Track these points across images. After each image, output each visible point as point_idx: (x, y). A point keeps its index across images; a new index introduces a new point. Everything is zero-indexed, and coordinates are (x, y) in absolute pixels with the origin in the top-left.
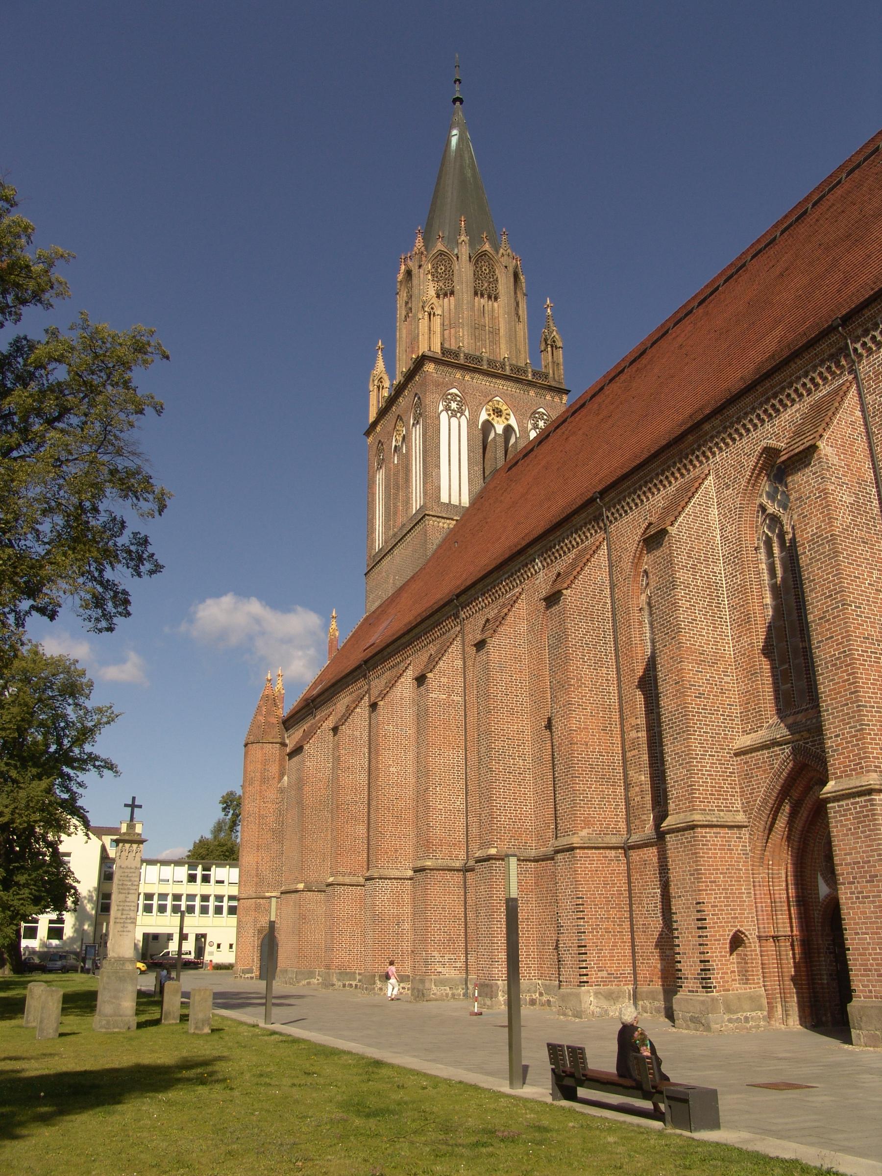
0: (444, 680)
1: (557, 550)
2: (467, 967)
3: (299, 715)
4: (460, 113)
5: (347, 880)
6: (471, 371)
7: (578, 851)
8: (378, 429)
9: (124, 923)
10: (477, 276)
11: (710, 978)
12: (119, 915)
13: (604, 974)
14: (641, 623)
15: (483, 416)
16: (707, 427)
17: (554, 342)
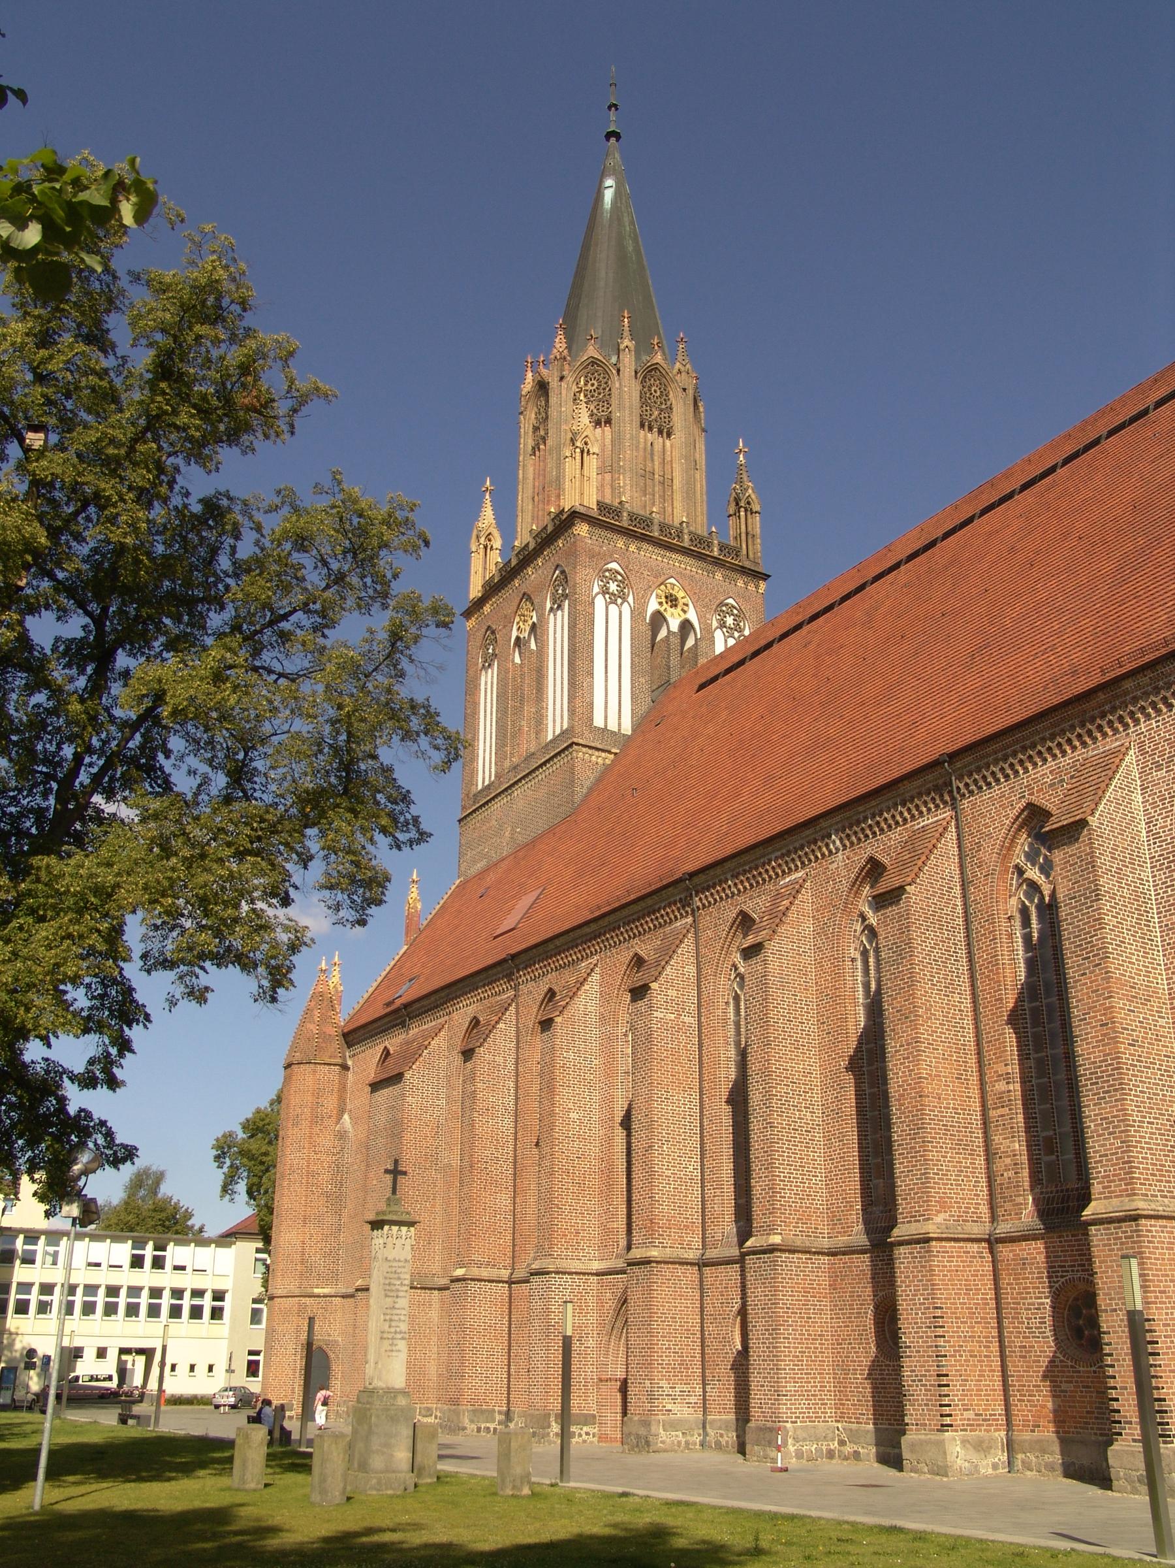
0: (672, 993)
1: (870, 826)
2: (704, 1404)
3: (375, 1025)
4: (617, 155)
5: (485, 1273)
6: (636, 538)
7: (934, 1243)
8: (487, 609)
9: (393, 1338)
10: (644, 400)
11: (1168, 1424)
12: (386, 1328)
13: (970, 1414)
14: (1010, 936)
15: (653, 606)
16: (1128, 685)
17: (749, 503)
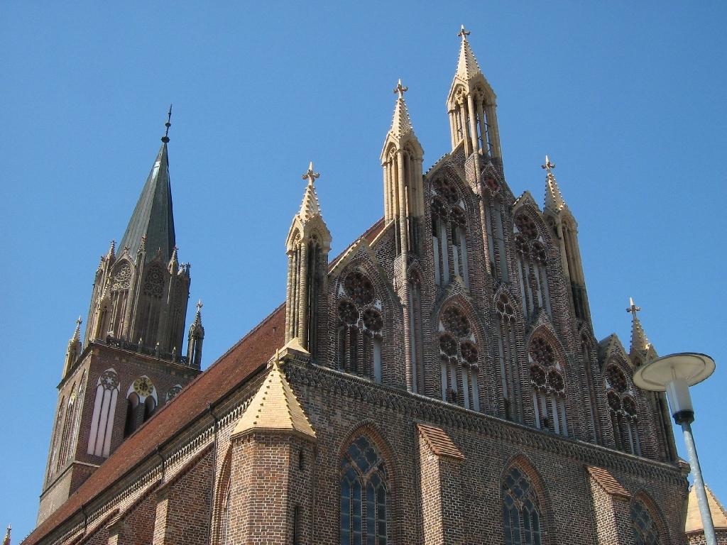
15: (132, 389)
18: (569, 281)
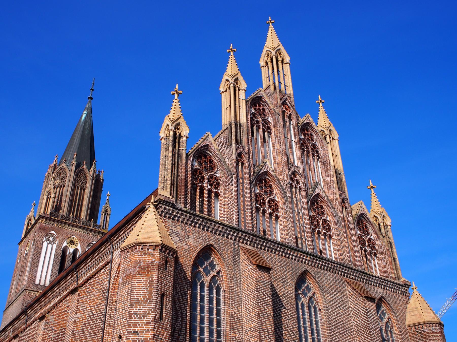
6: (62, 223)
15: (65, 244)
18: (334, 168)
